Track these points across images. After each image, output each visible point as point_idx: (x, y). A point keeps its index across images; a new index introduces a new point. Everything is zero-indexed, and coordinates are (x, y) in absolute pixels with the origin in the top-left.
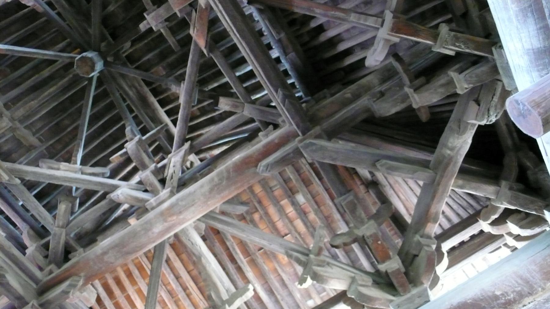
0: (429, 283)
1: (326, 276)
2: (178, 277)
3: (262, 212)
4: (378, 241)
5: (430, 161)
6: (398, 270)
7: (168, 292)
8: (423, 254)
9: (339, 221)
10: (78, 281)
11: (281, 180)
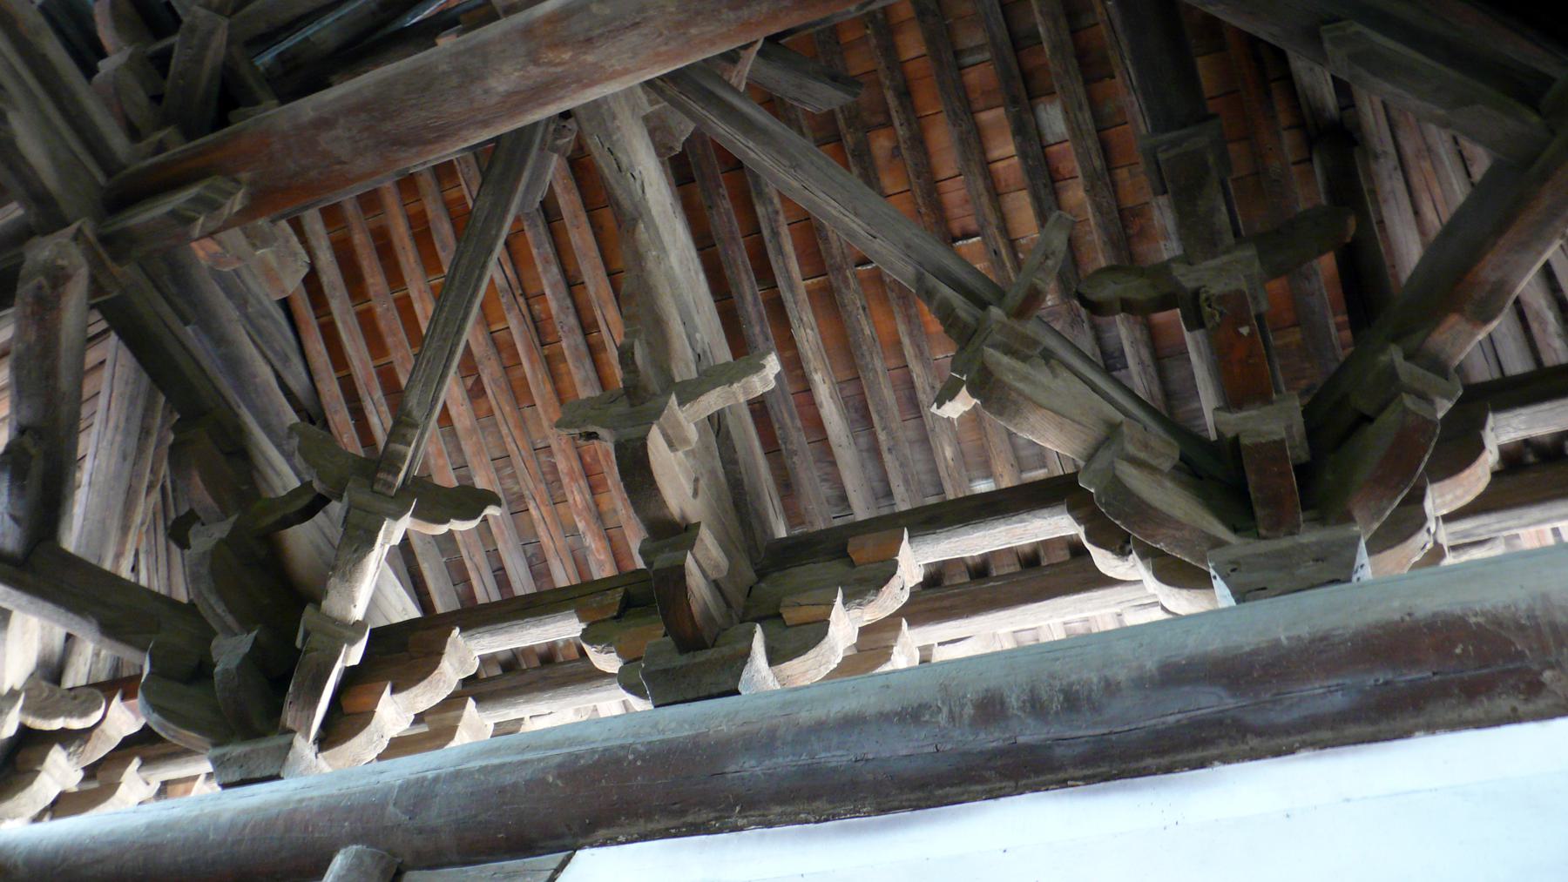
0: (1376, 526)
1: (1020, 393)
2: (572, 283)
3: (902, 132)
4: (1242, 325)
5: (1548, 81)
6: (1279, 445)
7: (534, 321)
8: (1389, 420)
9: (1166, 237)
10: (230, 194)
11: (1002, 34)
